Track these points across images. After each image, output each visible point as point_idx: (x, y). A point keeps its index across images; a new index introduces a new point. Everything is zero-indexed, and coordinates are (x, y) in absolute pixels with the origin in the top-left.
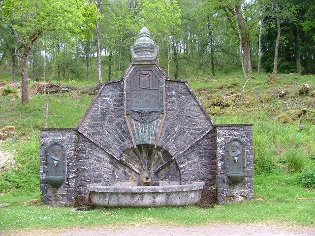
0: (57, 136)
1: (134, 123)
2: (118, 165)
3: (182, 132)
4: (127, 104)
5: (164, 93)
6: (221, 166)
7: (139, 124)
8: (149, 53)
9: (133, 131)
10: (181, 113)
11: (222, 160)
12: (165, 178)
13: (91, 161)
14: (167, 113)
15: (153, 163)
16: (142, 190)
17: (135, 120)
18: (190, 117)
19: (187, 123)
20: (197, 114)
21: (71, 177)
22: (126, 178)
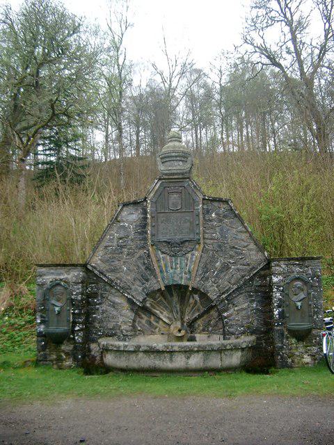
0: (59, 274)
1: (161, 256)
2: (140, 313)
3: (226, 267)
4: (151, 232)
5: (201, 216)
6: (279, 314)
7: (168, 258)
8: (181, 163)
9: (160, 267)
10: (224, 243)
11: (279, 306)
12: (203, 330)
13: (104, 307)
14: (204, 243)
15: (188, 310)
16: (170, 347)
17: (163, 253)
18: (236, 248)
19: (231, 257)
20: (246, 244)
21: (77, 328)
22: (152, 329)
